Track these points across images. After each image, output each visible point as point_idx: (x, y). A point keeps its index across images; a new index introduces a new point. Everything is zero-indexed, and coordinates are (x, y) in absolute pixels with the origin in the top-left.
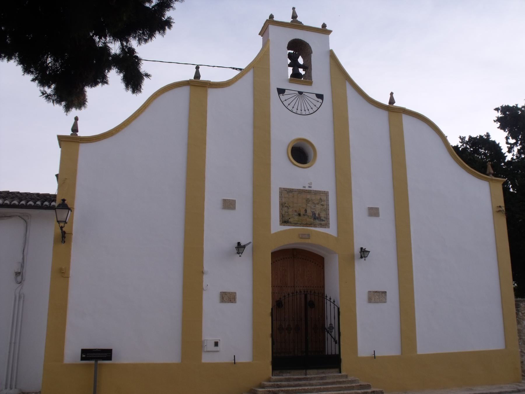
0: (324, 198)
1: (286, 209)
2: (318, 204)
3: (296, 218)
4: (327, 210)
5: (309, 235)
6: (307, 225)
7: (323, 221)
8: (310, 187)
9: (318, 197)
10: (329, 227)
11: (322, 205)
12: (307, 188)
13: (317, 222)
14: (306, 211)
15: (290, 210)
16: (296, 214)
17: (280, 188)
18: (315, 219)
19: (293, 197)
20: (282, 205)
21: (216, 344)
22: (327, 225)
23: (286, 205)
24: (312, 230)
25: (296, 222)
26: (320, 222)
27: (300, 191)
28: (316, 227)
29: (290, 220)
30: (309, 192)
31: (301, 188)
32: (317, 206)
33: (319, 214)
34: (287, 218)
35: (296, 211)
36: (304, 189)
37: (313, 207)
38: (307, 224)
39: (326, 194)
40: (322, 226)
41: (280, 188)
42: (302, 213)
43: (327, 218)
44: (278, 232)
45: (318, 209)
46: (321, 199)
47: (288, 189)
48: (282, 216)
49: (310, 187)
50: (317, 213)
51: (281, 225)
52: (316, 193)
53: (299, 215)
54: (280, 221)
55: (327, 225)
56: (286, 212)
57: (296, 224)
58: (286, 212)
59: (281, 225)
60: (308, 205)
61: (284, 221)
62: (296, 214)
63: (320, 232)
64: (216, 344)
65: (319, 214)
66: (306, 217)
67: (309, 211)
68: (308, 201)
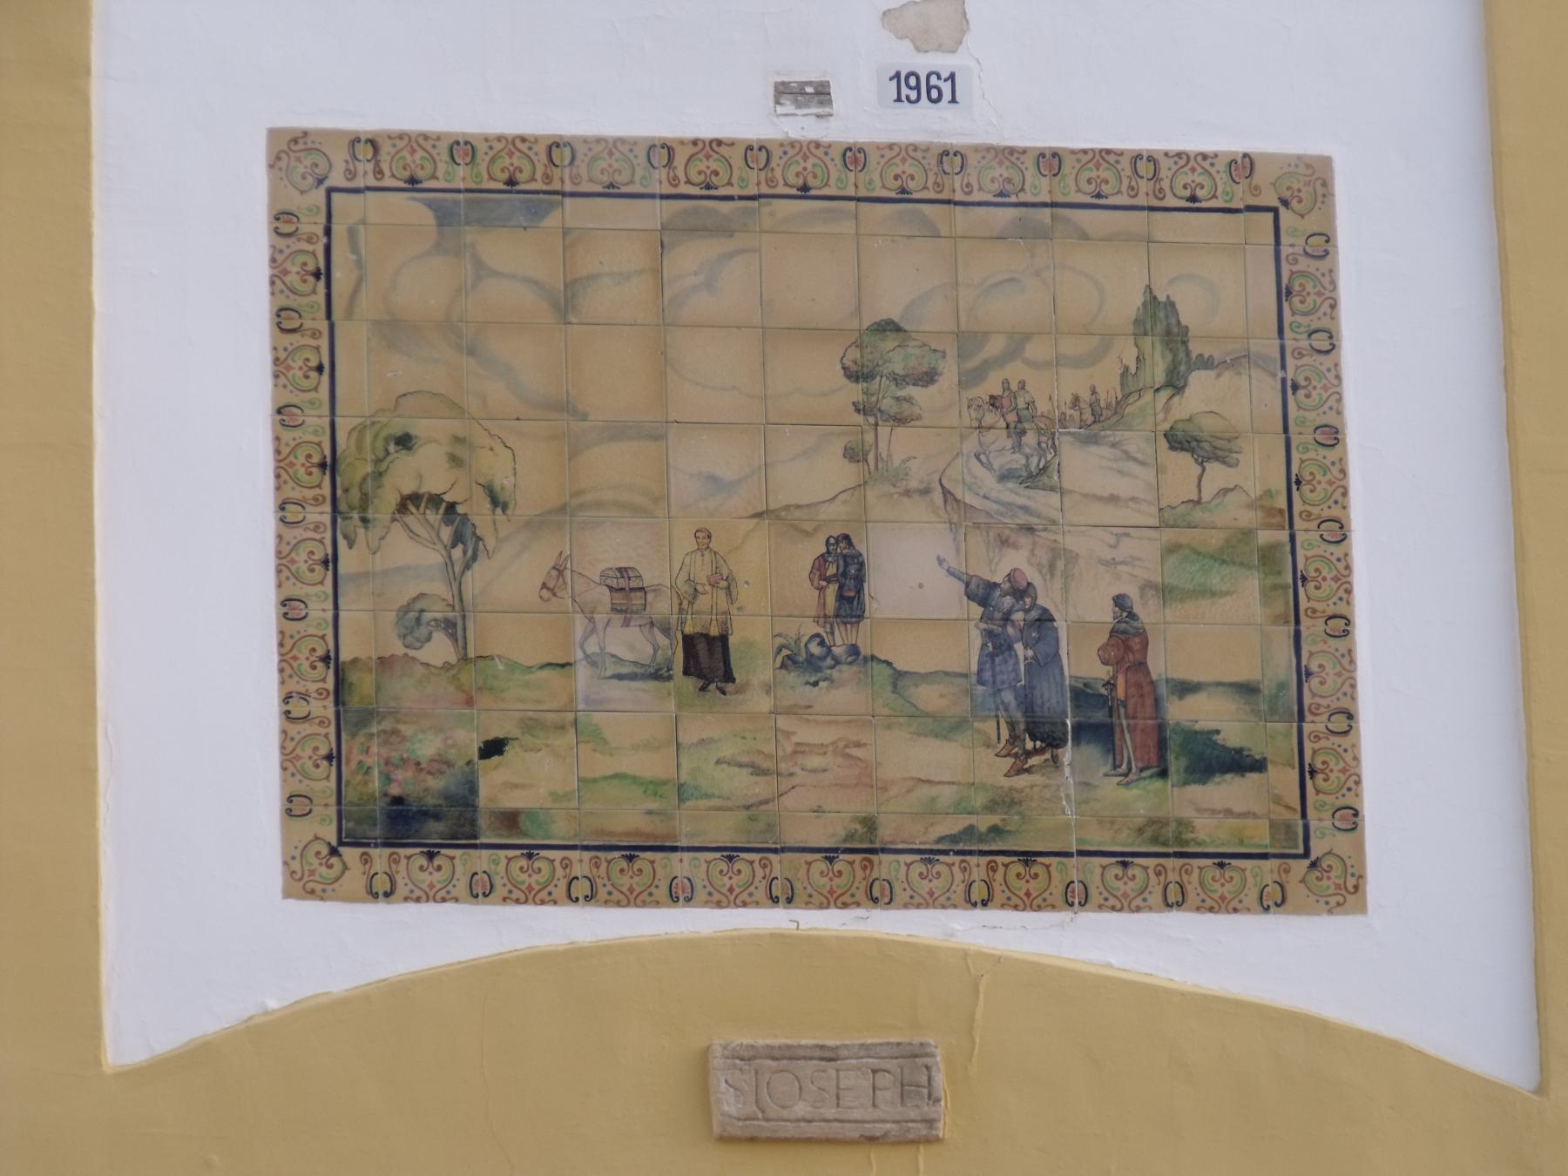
0: (1221, 288)
1: (409, 557)
2: (1098, 419)
3: (640, 730)
4: (1296, 557)
5: (910, 1069)
6: (860, 861)
7: (1215, 760)
8: (913, 87)
9: (1104, 281)
10: (1344, 889)
11: (1181, 441)
12: (863, 117)
13: (1083, 794)
14: (845, 575)
15: (510, 574)
16: (630, 643)
17: (292, 149)
18: (1038, 735)
19: (565, 302)
20: (333, 484)
21: (921, 586)
22: (1305, 855)
23: (424, 470)
24: (971, 969)
25: (629, 816)
26: (1142, 799)
27: (706, 187)
28: (1076, 898)
29: (497, 786)
30: (921, 187)
31: (747, 117)
32: (1083, 466)
33: (1126, 640)
34: (432, 741)
35: (626, 590)
36: (800, 126)
37: (984, 486)
38: (865, 845)
39: (1280, 209)
40: (1168, 869)
41: (292, 149)
42: (753, 639)
43: (1308, 720)
44: (260, 1034)
45: (1103, 533)
46: (1158, 319)
47: (462, 148)
48: (334, 695)
49: (913, 87)
50: (1081, 611)
51: (305, 880)
52: (1065, 193)
53: (708, 660)
54: (294, 806)
55: (1305, 855)
56: (412, 621)
57: (628, 860)
58: (412, 621)
59: (305, 880)
60: (898, 445)
61: (387, 811)
62: (630, 643)
63: (1149, 999)
64: (921, 586)
65: (1126, 640)
66: (843, 694)
67: (917, 578)
68: (879, 365)
